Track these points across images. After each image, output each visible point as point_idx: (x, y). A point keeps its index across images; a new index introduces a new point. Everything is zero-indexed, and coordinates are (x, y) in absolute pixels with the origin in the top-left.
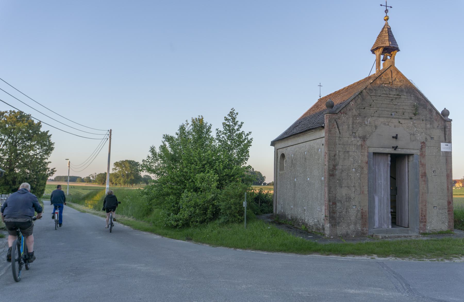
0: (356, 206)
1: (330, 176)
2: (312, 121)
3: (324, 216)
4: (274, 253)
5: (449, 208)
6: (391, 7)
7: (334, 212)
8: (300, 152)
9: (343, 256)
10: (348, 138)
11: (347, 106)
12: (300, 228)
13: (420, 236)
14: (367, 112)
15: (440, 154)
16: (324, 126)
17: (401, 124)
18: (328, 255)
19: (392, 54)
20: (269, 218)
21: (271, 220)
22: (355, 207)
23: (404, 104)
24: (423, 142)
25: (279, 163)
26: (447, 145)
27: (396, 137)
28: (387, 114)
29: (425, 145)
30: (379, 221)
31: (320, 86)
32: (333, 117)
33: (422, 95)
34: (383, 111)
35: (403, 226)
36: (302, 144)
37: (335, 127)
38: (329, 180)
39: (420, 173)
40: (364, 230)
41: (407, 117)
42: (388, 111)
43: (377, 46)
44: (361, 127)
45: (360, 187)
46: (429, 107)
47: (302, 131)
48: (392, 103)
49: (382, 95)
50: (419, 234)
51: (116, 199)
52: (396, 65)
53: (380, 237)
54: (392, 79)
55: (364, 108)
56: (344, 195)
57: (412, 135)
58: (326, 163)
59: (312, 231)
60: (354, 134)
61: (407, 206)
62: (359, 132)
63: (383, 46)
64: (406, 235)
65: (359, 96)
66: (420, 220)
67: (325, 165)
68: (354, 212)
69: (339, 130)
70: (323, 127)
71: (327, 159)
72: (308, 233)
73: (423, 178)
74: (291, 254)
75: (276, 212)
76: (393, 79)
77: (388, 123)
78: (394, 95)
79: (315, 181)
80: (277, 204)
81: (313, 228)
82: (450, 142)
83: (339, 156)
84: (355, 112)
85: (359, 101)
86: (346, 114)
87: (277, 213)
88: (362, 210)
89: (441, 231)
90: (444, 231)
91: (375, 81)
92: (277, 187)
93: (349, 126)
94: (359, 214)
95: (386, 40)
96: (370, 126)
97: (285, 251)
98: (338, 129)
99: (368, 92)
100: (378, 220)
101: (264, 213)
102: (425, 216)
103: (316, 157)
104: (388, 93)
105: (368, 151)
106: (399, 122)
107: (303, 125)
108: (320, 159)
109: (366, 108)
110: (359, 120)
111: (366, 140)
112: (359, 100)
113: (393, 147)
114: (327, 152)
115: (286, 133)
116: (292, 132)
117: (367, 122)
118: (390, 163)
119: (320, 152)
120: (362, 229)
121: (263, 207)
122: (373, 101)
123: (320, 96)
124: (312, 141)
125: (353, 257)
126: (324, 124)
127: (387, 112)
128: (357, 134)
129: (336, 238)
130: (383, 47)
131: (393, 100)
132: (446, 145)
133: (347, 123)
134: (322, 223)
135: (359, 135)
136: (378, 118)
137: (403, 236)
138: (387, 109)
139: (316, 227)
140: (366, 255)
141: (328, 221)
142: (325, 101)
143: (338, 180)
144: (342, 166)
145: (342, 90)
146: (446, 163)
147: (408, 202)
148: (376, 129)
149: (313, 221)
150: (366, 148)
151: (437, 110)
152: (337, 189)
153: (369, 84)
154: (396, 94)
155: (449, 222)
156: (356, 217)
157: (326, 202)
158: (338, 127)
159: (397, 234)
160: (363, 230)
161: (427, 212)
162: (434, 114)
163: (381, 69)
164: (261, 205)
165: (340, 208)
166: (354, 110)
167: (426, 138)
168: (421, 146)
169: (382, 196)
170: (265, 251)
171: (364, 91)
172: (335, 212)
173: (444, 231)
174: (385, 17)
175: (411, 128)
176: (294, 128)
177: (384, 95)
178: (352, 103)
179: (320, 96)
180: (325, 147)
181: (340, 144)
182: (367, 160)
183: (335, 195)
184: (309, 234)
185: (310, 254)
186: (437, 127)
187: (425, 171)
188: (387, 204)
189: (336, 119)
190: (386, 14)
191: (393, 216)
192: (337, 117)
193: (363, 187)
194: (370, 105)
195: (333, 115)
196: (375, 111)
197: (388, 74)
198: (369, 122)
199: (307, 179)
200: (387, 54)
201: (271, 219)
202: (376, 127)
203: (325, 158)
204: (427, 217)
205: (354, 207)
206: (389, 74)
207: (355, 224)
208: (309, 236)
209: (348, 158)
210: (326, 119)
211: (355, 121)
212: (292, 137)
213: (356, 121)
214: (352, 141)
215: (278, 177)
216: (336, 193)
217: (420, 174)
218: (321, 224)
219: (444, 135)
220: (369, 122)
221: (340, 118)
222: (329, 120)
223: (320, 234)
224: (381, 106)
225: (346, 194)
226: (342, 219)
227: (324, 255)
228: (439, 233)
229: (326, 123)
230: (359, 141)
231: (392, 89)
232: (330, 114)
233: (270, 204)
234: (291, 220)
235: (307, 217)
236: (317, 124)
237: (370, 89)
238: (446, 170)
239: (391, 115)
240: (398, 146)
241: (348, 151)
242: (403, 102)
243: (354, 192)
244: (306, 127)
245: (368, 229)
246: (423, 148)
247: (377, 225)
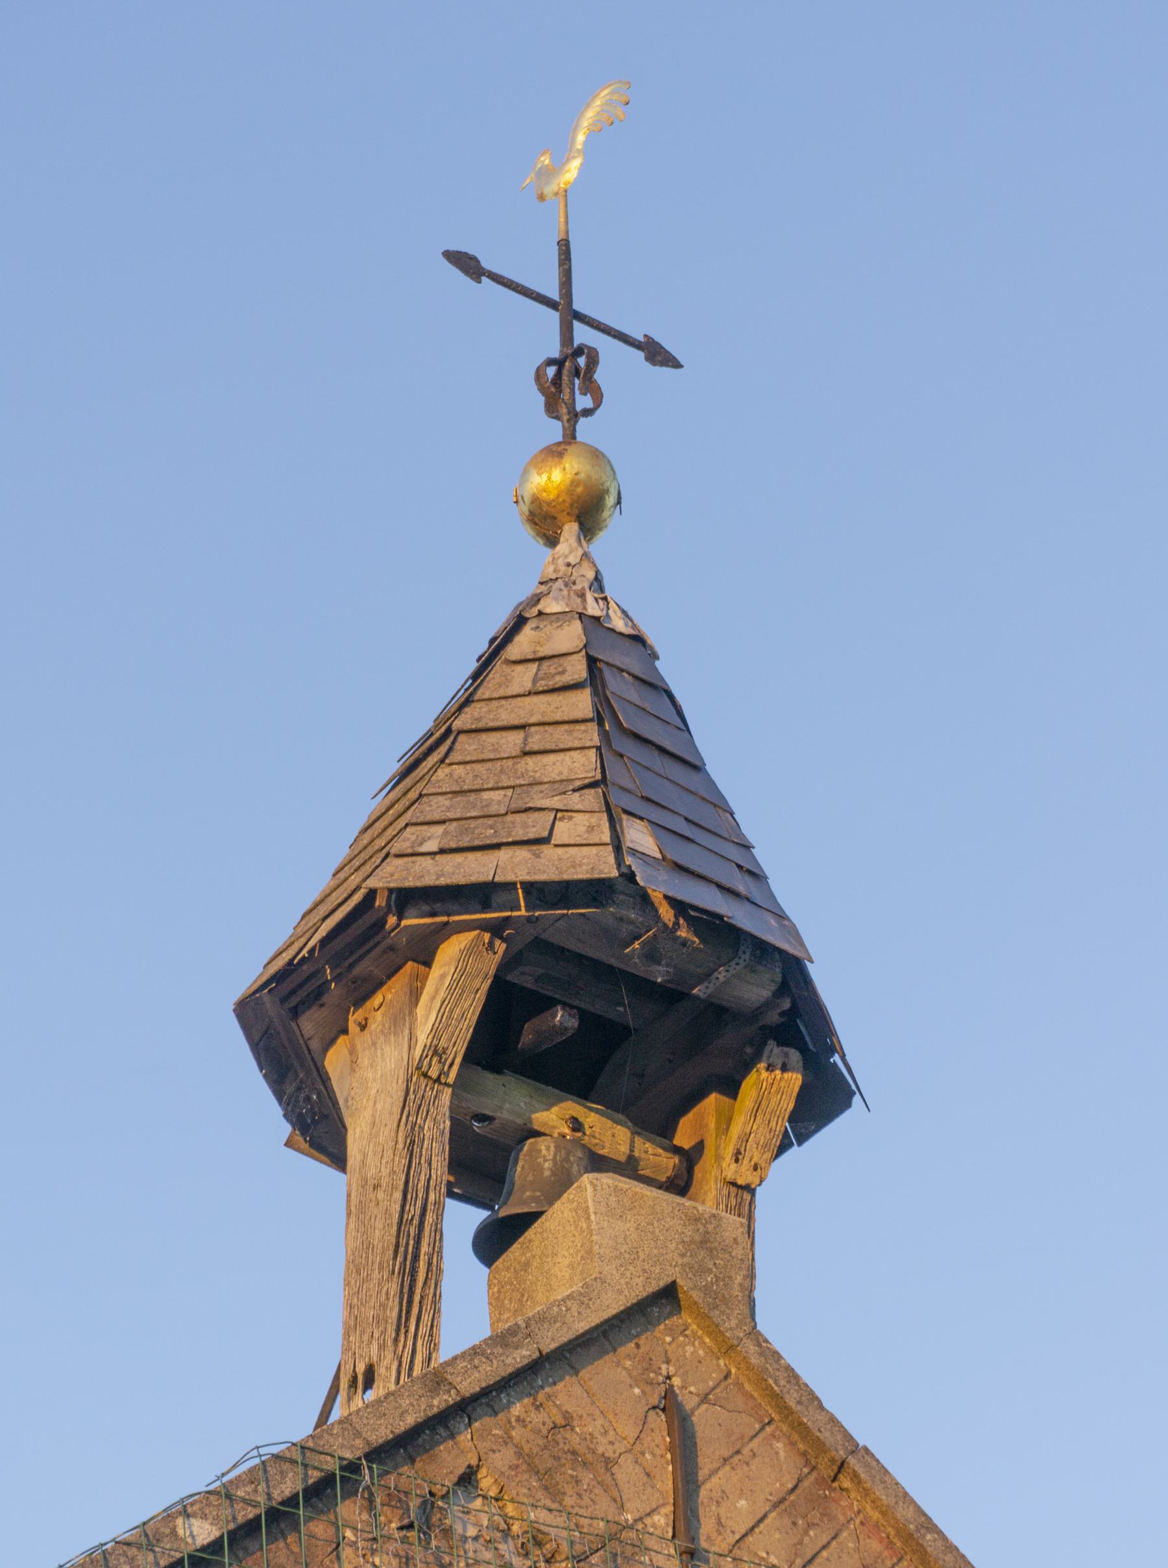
6: (656, 354)
19: (690, 1158)
206: (627, 1472)
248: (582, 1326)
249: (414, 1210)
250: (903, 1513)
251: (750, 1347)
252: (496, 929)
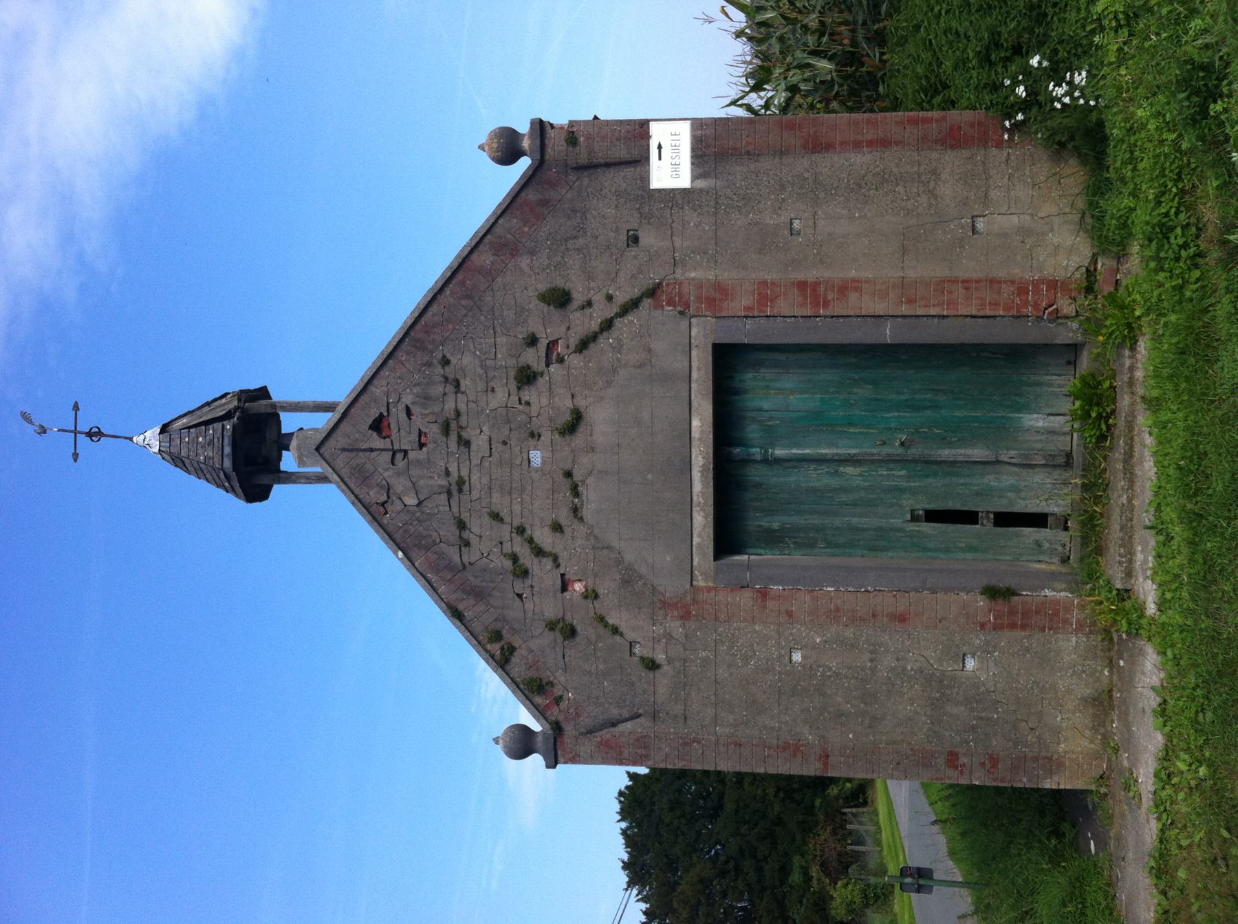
26: (660, 147)
29: (668, 285)
120: (1077, 631)
191: (561, 759)
204: (1028, 276)
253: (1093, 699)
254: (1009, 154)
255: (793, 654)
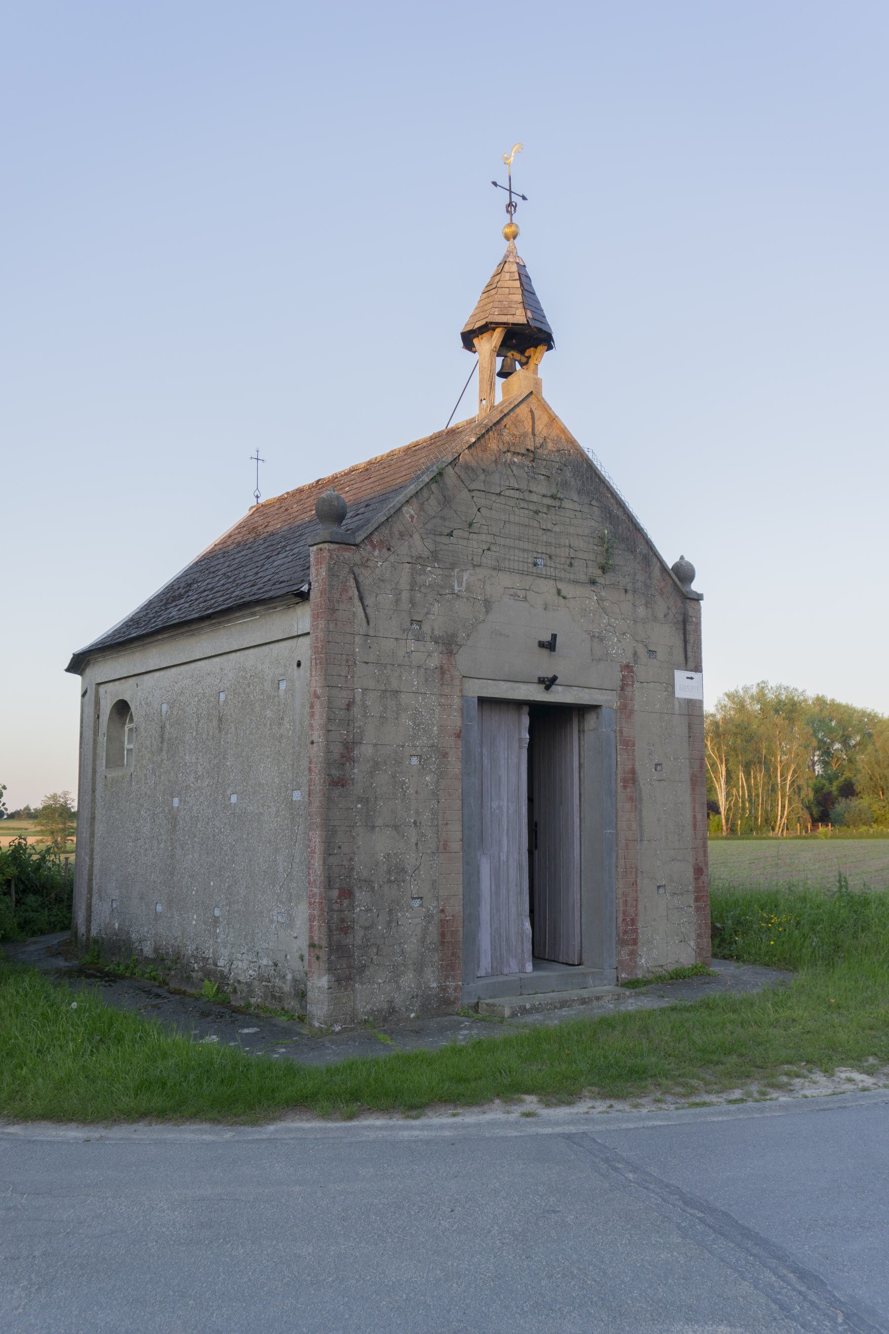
0: (421, 898)
1: (330, 785)
2: (245, 577)
3: (302, 943)
4: (115, 1128)
5: (698, 889)
7: (345, 929)
8: (197, 695)
9: (414, 1113)
10: (397, 639)
11: (394, 519)
12: (191, 990)
13: (628, 993)
14: (460, 546)
15: (673, 708)
16: (309, 589)
17: (564, 598)
18: (351, 1117)
19: (529, 358)
20: (55, 953)
21: (67, 964)
22: (418, 902)
23: (572, 530)
24: (627, 666)
25: (102, 740)
26: (692, 678)
27: (550, 646)
28: (519, 561)
30: (491, 949)
31: (258, 459)
32: (342, 558)
33: (621, 505)
34: (510, 547)
35: (561, 960)
36: (206, 661)
37: (351, 598)
38: (329, 802)
39: (619, 772)
40: (448, 986)
41: (583, 578)
42: (524, 550)
43: (488, 320)
44: (438, 601)
45: (437, 826)
46: (642, 548)
47: (211, 611)
48: (536, 524)
49: (507, 493)
50: (617, 985)
51: (81, 656)
52: (547, 394)
53: (507, 1012)
54: (534, 441)
55: (450, 535)
56: (381, 857)
57: (596, 640)
58: (317, 735)
59: (249, 1005)
60: (415, 627)
61: (576, 888)
62: (433, 620)
63: (505, 321)
64: (585, 993)
65: (434, 487)
66: (621, 935)
67: (312, 743)
68: (418, 920)
69: (364, 610)
70: (304, 597)
71: (319, 721)
72: (233, 1012)
73: (628, 790)
74: (193, 1127)
75: (89, 930)
76: (539, 440)
77: (524, 592)
78: (544, 496)
79: (263, 806)
80: (94, 900)
81: (251, 993)
82: (698, 669)
83: (364, 706)
84: (419, 545)
85: (433, 505)
86: (389, 549)
87: (94, 933)
88: (442, 911)
89: (676, 969)
90: (686, 967)
91: (482, 441)
92: (96, 831)
93: (398, 593)
94: (433, 930)
95: (516, 302)
96: (467, 599)
97: (162, 1115)
98: (360, 604)
99: (463, 475)
100: (491, 943)
101: (34, 934)
102: (633, 922)
103: (269, 713)
104: (523, 486)
105: (461, 691)
106: (559, 592)
107: (206, 593)
108: (286, 719)
109: (455, 533)
110: (432, 575)
111: (455, 648)
112: (433, 502)
113: (539, 678)
114: (319, 691)
115: (133, 622)
116: (160, 616)
117: (460, 584)
118: (528, 736)
119: (286, 691)
121: (26, 911)
122: (479, 510)
123: (257, 497)
124: (252, 650)
125: (454, 1115)
126: (310, 584)
127: (521, 555)
128: (426, 628)
129: (352, 1030)
130: (504, 324)
131: (541, 514)
132: (688, 678)
133: (394, 586)
134: (293, 972)
135: (433, 630)
136: (494, 573)
137: (578, 999)
138: (522, 545)
139: (266, 986)
140: (497, 1101)
141: (324, 965)
142: (283, 512)
143: (360, 800)
144: (375, 745)
145: (346, 474)
146: (690, 737)
147: (579, 874)
148: (487, 612)
149: (252, 965)
150: (457, 682)
151: (663, 561)
152: (358, 835)
153: (464, 448)
154: (549, 494)
155: (699, 936)
156: (423, 940)
157: (315, 890)
158: (361, 599)
159: (553, 991)
160: (443, 989)
161: (641, 907)
162: (657, 572)
163: (496, 404)
164: (18, 902)
165: (368, 910)
166: (416, 537)
167: (635, 654)
168: (622, 680)
169: (503, 857)
170: (71, 1120)
171: (450, 470)
172: (348, 927)
173: (685, 970)
174: (504, 228)
175: (594, 615)
176: (165, 604)
177: (512, 493)
178: (408, 512)
179: (257, 497)
180: (314, 673)
181: (367, 663)
182: (459, 724)
183: (351, 859)
184: (240, 1017)
185: (274, 1120)
186: (665, 616)
187: (634, 765)
188: (516, 885)
189: (355, 565)
190: (508, 216)
192: (357, 558)
193: (447, 824)
194: (470, 525)
195: (346, 550)
196: (485, 547)
197: (523, 421)
198: (464, 584)
199: (230, 799)
200: (515, 353)
201: (66, 960)
202: (488, 604)
203: (312, 715)
205: (416, 904)
206: (526, 422)
207: (419, 969)
208: (243, 1027)
209: (395, 716)
210: (318, 562)
211: (420, 579)
212: (165, 636)
213: (423, 577)
214: (409, 654)
215: (97, 792)
216: (354, 853)
217: (619, 776)
218: (289, 977)
219: (682, 645)
220: (464, 584)
221: (369, 563)
222: (330, 570)
223: (284, 1018)
224: (502, 530)
225: (389, 855)
226: (375, 951)
227: (336, 1120)
228: (672, 978)
229: (317, 581)
230: (433, 652)
231: (536, 476)
232: (333, 546)
233: (53, 895)
234: (153, 961)
235: (225, 947)
236: (274, 584)
237: (467, 467)
238: (690, 762)
239: (535, 564)
240: (557, 675)
241: (397, 692)
242: (570, 525)
243: (417, 844)
244: (221, 599)
245: (460, 983)
246: (627, 685)
247: (486, 963)
248: (520, 400)
249: (491, 374)
250: (562, 426)
251: (542, 401)
252: (505, 328)
253: (394, 1007)
254: (692, 907)
255: (416, 758)
